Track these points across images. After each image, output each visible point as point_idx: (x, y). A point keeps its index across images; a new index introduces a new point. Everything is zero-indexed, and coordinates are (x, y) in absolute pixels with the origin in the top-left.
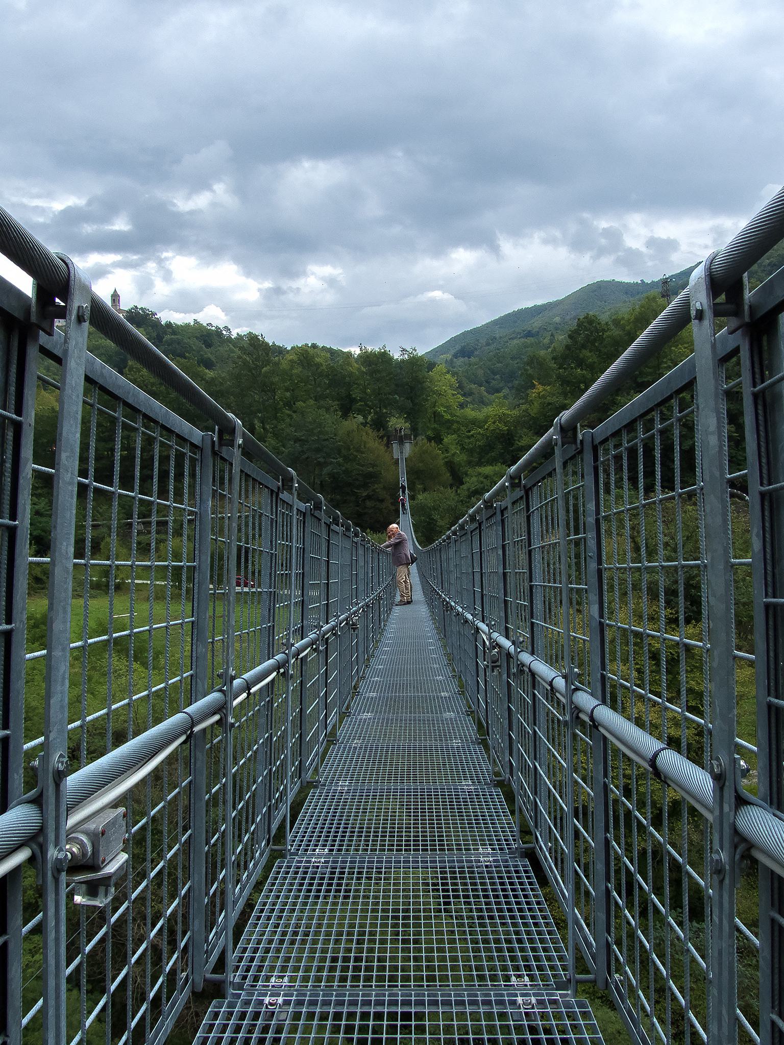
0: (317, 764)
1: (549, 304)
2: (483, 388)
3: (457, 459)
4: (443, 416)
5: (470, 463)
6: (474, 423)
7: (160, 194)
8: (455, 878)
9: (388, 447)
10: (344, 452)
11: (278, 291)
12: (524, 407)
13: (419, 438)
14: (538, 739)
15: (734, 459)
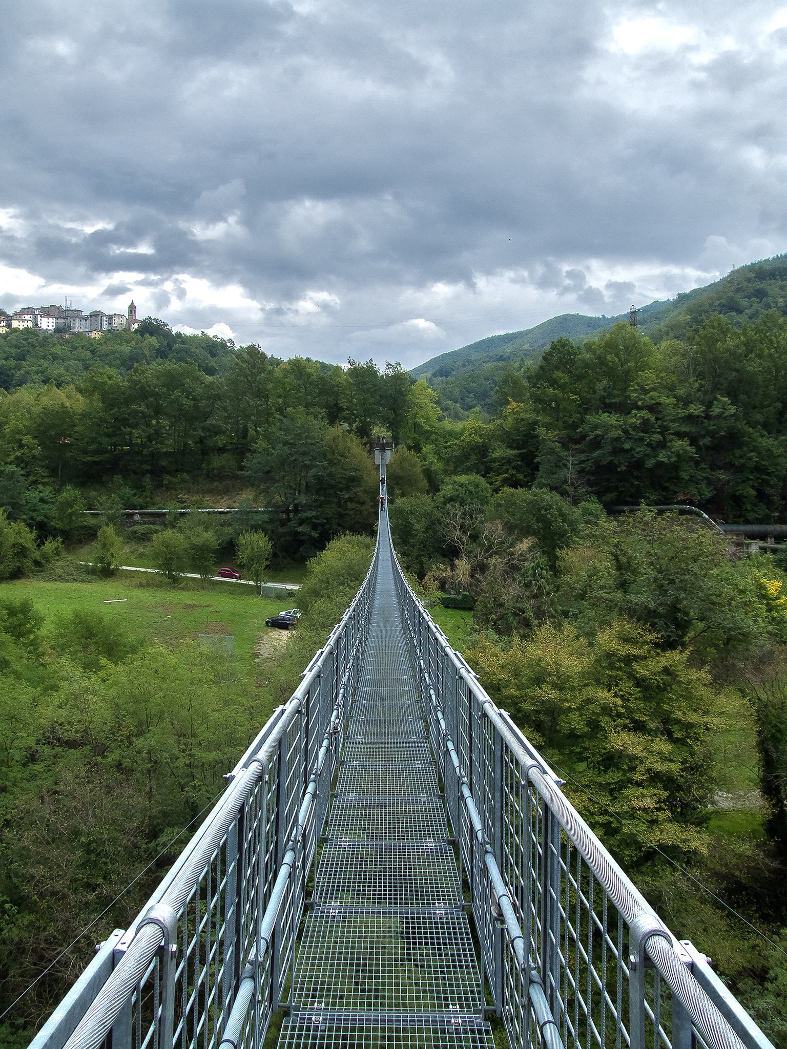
1: (521, 333)
2: (458, 405)
3: (433, 468)
4: (422, 427)
5: (445, 471)
6: (451, 434)
7: (182, 225)
10: (329, 456)
11: (279, 311)
12: (499, 421)
13: (400, 447)
14: (549, 853)
15: (693, 478)
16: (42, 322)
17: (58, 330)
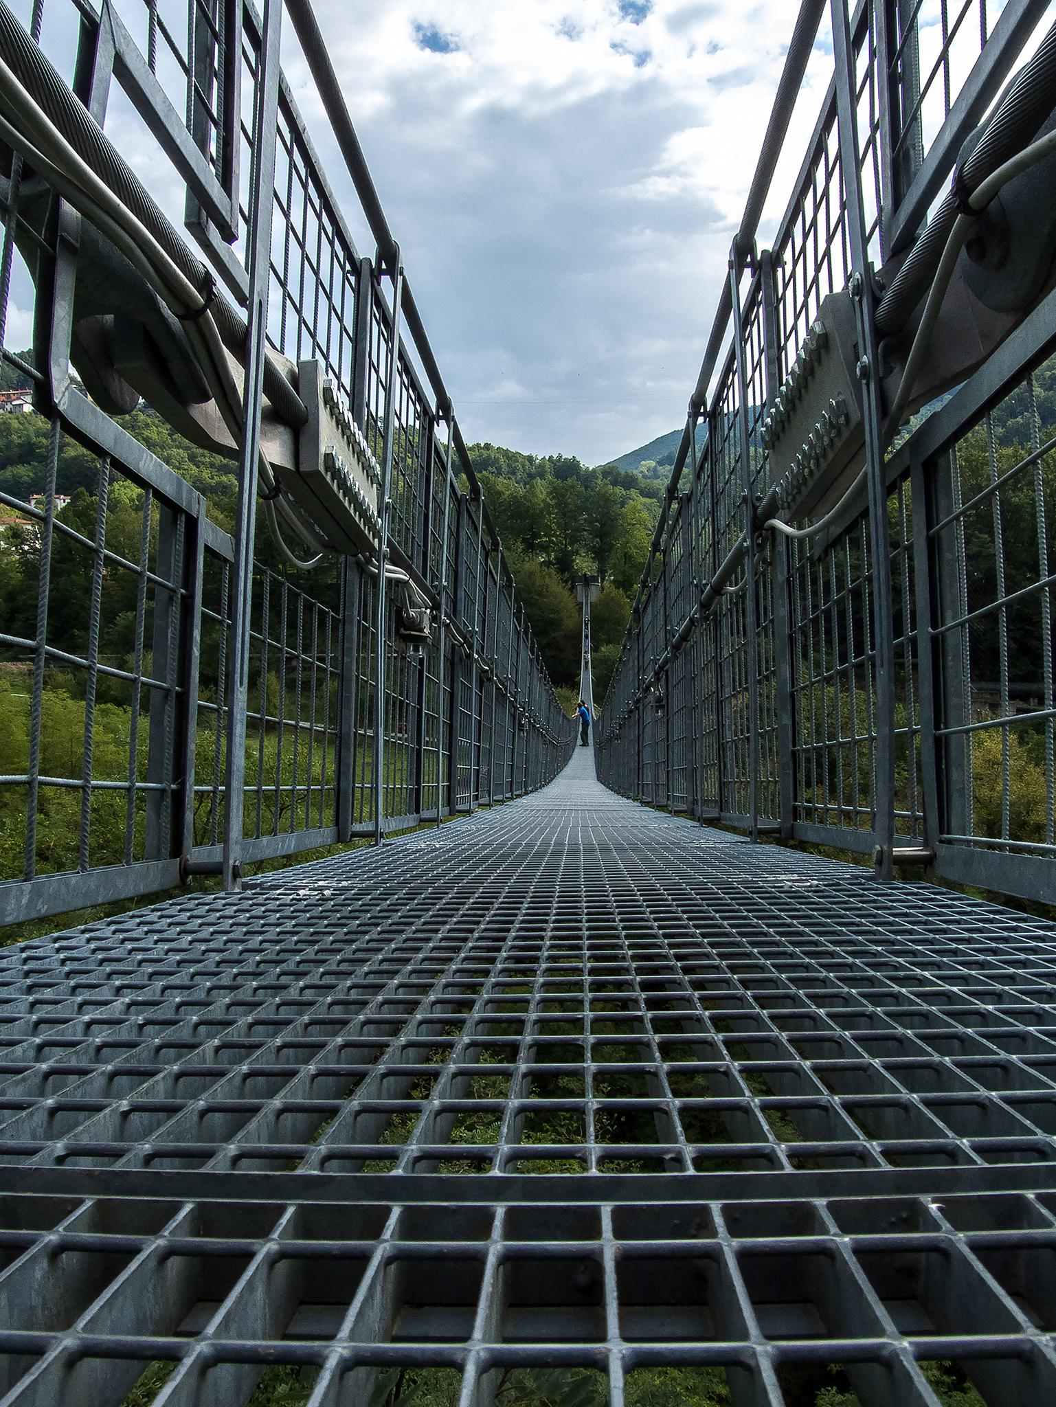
9: (572, 592)
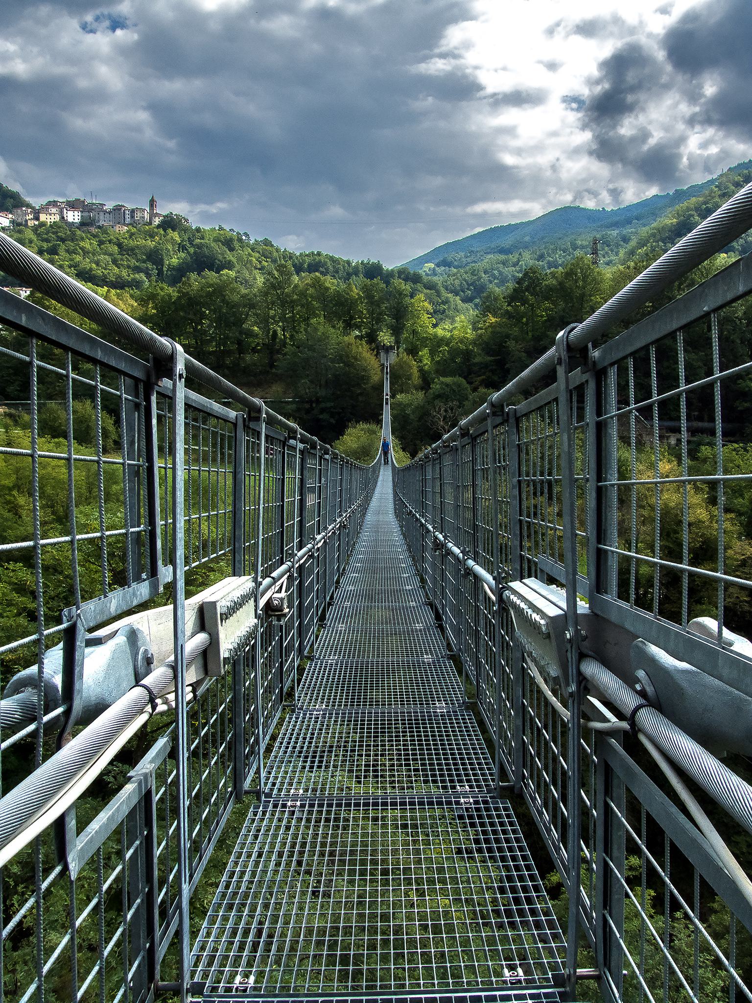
0: (313, 642)
8: (412, 750)
16: (68, 215)
17: (83, 224)
